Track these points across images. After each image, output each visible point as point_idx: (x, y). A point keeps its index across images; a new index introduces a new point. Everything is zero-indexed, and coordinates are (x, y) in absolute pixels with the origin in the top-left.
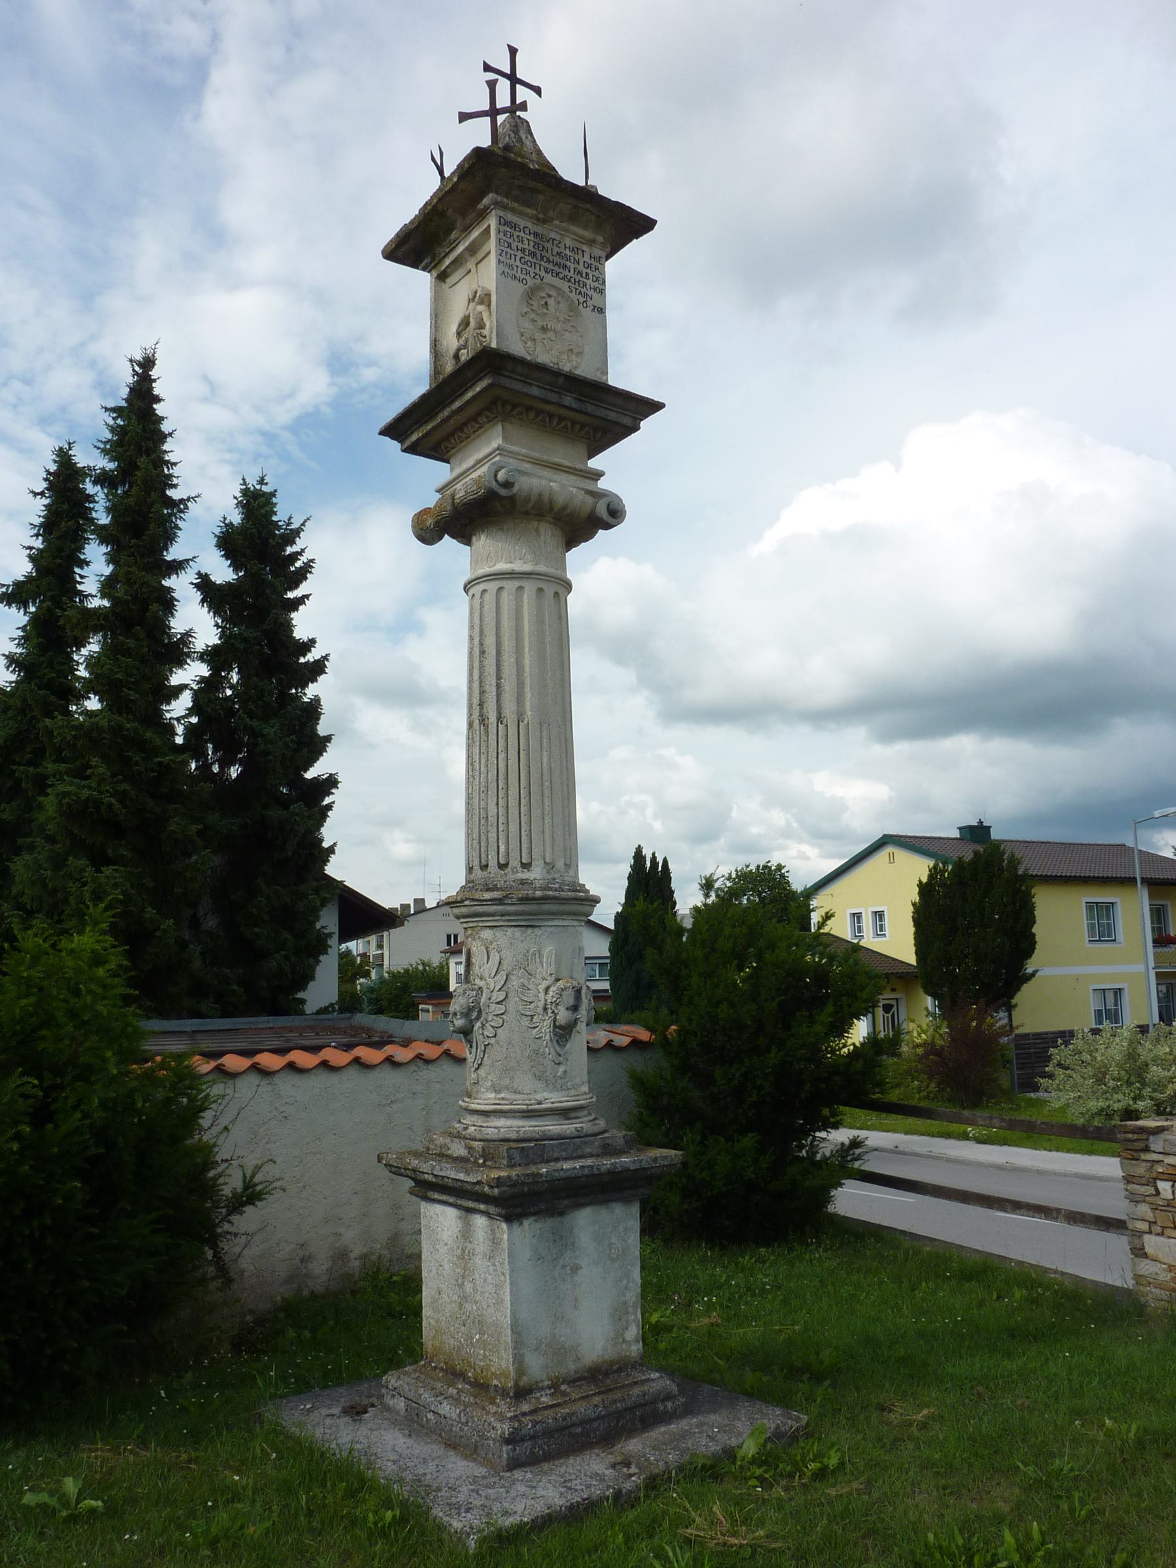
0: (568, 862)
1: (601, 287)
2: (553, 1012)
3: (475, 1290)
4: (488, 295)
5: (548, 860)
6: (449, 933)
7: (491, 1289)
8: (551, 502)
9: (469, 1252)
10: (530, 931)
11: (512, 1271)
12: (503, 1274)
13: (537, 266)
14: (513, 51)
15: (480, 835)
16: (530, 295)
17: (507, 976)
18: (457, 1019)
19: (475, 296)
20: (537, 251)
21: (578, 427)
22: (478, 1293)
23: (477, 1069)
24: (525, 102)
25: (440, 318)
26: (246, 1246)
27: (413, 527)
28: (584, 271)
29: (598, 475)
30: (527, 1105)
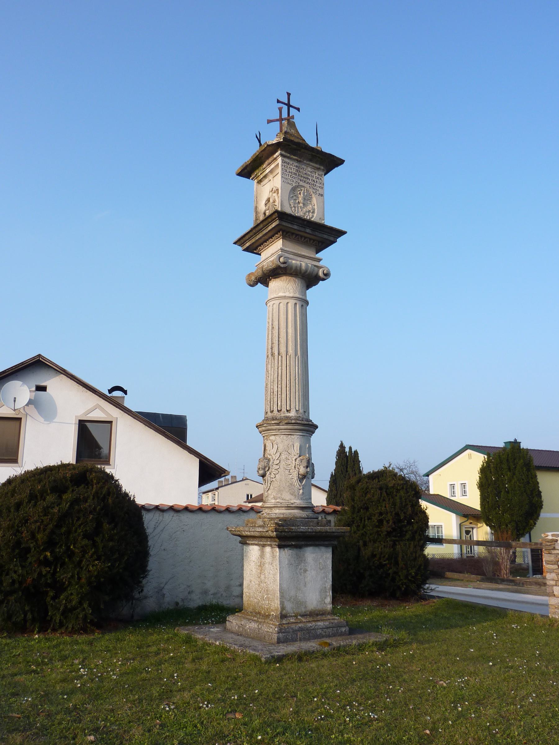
0: (305, 411)
1: (322, 186)
2: (298, 468)
3: (265, 578)
4: (278, 190)
5: (297, 409)
6: (248, 493)
7: (271, 576)
8: (309, 651)
9: (263, 563)
10: (290, 436)
11: (280, 568)
12: (276, 569)
13: (297, 178)
14: (289, 94)
15: (270, 399)
16: (294, 189)
17: (280, 454)
19: (272, 190)
20: (297, 173)
21: (312, 241)
22: (267, 579)
23: (268, 491)
24: (293, 116)
25: (258, 198)
26: (166, 584)
28: (316, 180)
29: (319, 260)
30: (287, 505)
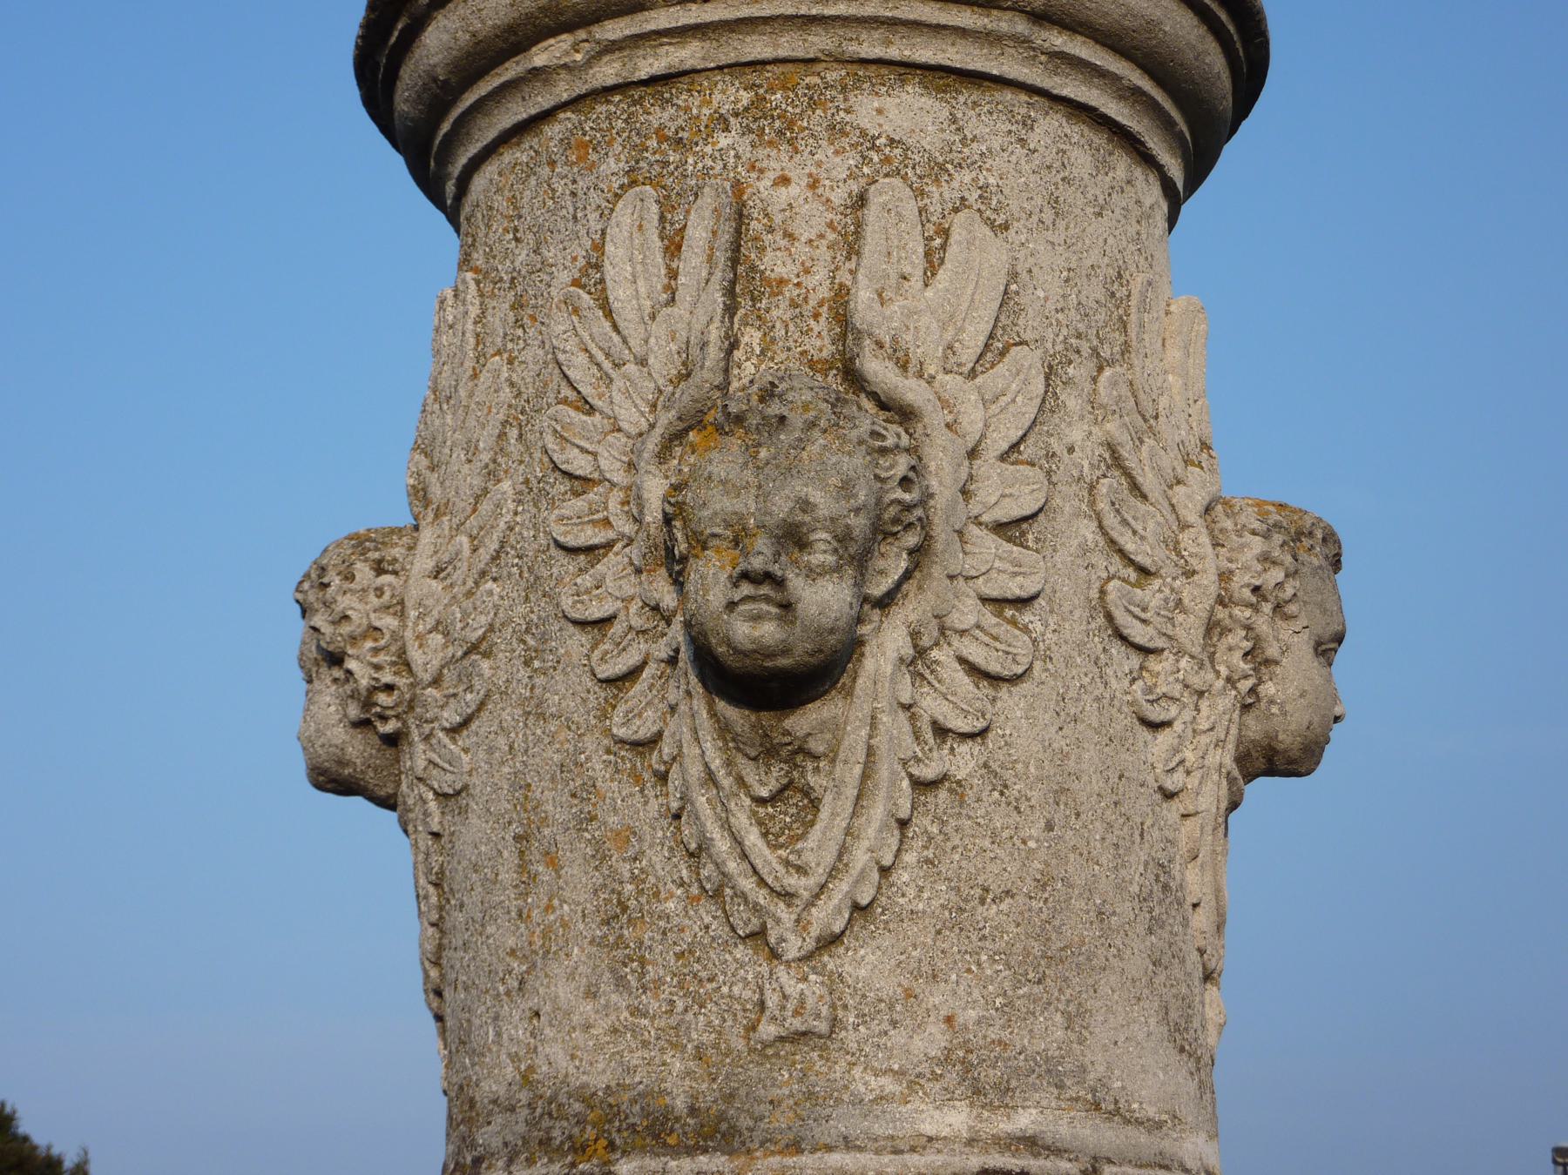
18: (812, 574)
27: (311, 782)
